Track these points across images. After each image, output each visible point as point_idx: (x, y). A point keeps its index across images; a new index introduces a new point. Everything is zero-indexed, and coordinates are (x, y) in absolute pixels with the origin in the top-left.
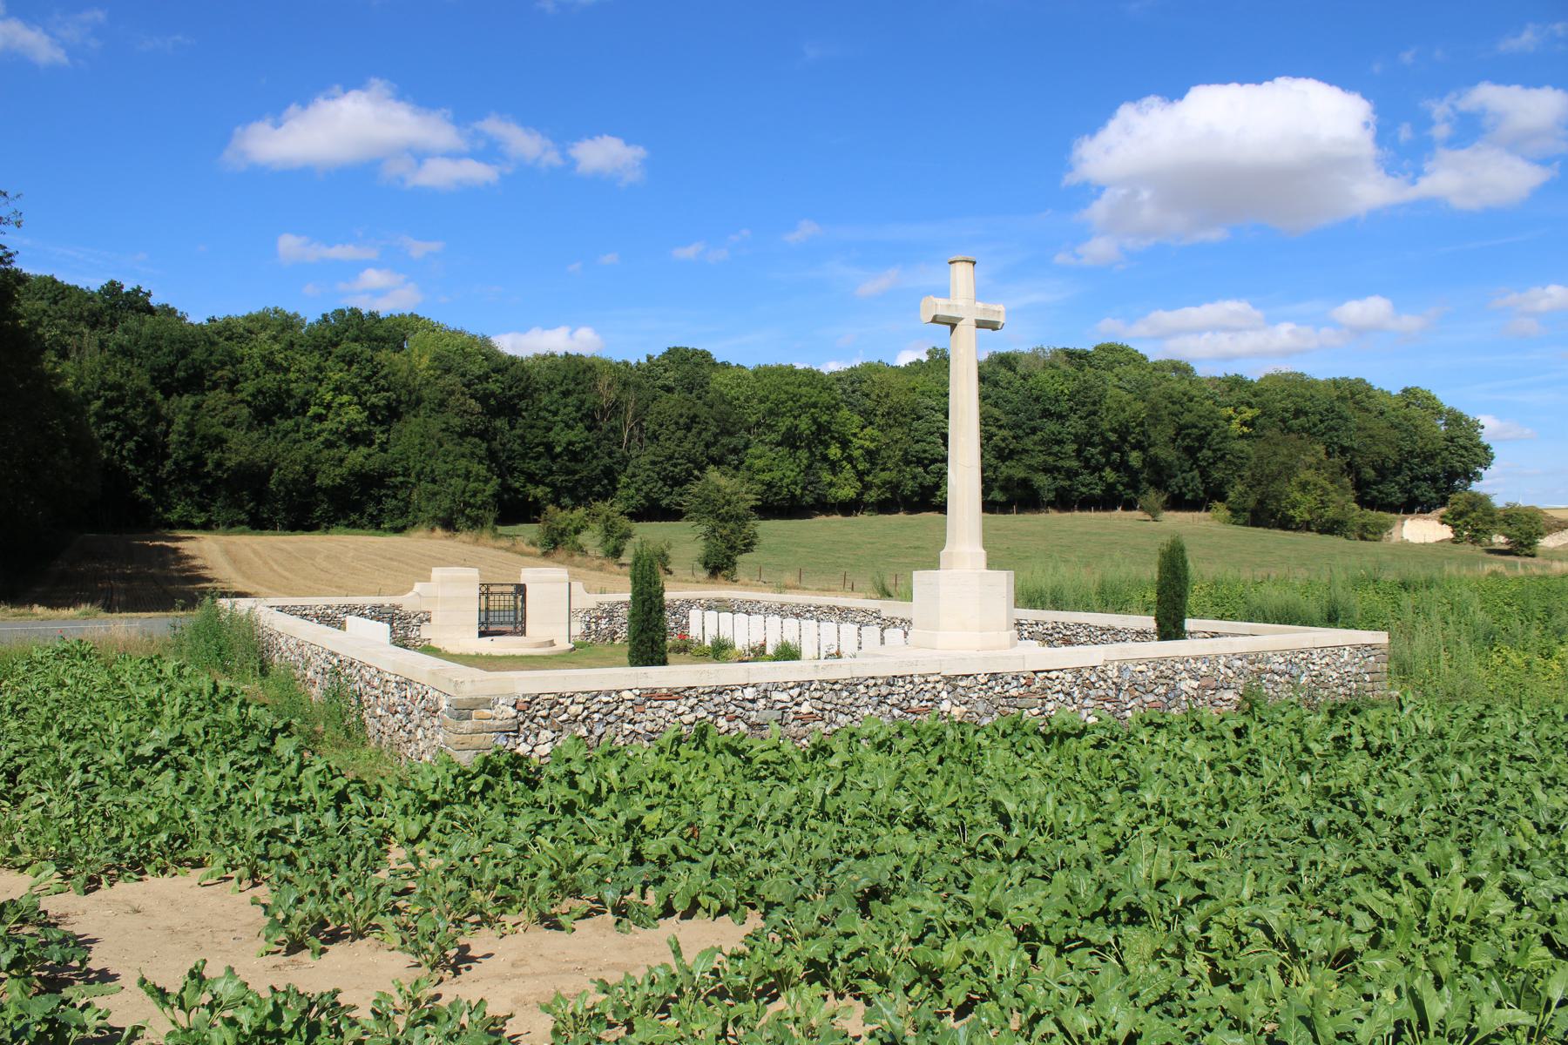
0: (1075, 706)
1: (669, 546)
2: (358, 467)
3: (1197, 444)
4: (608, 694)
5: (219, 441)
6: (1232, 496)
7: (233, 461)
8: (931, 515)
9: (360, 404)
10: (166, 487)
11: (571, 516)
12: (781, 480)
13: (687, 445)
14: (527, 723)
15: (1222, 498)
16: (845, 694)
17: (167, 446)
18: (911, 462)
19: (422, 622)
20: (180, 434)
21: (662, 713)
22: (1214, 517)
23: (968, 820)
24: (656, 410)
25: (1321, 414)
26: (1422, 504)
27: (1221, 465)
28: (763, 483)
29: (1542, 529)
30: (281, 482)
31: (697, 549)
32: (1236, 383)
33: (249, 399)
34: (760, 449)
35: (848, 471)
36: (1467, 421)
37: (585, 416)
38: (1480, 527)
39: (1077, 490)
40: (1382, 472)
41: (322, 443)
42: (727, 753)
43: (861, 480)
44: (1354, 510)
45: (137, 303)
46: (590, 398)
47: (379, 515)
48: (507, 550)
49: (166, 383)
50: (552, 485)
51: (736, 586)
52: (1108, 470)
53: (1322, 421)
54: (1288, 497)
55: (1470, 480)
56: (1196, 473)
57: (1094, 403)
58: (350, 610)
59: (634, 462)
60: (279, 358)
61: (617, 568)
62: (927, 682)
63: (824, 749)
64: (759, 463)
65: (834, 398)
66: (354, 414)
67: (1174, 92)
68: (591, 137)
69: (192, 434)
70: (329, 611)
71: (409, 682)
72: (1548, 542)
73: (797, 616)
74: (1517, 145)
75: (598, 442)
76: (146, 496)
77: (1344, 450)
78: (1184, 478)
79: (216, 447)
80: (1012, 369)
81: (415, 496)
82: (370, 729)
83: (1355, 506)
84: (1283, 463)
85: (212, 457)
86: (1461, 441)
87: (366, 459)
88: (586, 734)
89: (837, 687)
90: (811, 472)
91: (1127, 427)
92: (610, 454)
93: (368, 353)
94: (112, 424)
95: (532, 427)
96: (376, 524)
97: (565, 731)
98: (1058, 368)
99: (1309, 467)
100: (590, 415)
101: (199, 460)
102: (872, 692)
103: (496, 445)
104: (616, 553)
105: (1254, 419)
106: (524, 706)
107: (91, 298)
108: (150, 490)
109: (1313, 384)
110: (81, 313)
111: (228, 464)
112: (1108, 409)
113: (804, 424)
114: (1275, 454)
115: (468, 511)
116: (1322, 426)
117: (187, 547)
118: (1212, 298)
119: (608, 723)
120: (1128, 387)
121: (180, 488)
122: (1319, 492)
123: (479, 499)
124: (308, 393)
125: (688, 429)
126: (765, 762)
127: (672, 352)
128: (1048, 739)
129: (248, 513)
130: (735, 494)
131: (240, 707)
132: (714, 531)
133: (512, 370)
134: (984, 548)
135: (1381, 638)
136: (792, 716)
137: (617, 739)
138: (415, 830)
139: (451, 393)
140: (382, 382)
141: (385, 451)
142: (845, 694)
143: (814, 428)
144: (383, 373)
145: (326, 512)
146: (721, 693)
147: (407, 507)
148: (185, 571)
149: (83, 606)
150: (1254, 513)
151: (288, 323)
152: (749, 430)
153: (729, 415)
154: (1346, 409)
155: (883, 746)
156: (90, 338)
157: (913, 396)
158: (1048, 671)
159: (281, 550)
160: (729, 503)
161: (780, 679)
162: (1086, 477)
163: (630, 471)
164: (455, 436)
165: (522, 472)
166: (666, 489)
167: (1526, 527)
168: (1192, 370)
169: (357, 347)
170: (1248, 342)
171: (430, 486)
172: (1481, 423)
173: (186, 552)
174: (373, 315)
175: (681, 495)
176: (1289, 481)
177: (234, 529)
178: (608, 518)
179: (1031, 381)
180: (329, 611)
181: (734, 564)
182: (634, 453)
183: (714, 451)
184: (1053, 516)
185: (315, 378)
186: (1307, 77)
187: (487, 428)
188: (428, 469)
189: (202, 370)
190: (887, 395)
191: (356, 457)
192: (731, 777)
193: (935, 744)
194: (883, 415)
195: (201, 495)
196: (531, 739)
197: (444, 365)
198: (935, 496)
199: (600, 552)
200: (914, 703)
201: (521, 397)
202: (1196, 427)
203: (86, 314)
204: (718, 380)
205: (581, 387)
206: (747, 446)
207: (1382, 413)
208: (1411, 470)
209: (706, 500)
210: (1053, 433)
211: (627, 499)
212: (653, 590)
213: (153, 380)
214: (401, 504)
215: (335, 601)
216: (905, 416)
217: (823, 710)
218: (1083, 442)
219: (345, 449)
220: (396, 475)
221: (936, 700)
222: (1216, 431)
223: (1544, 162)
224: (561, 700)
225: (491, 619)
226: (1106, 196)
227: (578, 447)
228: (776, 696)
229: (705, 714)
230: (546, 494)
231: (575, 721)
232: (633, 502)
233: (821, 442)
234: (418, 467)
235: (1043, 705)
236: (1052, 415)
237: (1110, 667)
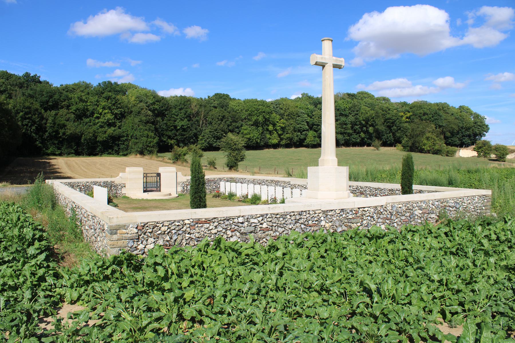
0: (374, 222)
1: (215, 160)
2: (111, 134)
3: (392, 125)
4: (179, 222)
5: (64, 126)
6: (403, 142)
7: (69, 132)
8: (303, 148)
10: (46, 141)
11: (183, 150)
12: (253, 137)
13: (221, 126)
14: (143, 235)
15: (400, 142)
16: (281, 219)
17: (46, 128)
18: (296, 131)
19: (122, 187)
20: (51, 123)
21: (203, 229)
22: (397, 149)
23: (348, 290)
24: (211, 114)
26: (465, 144)
27: (399, 131)
28: (247, 138)
29: (507, 152)
30: (85, 139)
31: (225, 160)
32: (405, 104)
33: (74, 112)
34: (246, 127)
35: (275, 134)
36: (480, 117)
37: (188, 116)
39: (351, 140)
40: (453, 134)
41: (99, 126)
42: (230, 251)
43: (280, 137)
44: (444, 146)
45: (36, 80)
46: (189, 111)
47: (119, 150)
48: (161, 161)
49: (46, 107)
50: (177, 139)
51: (238, 173)
53: (433, 117)
54: (422, 142)
55: (482, 136)
56: (391, 134)
57: (357, 111)
58: (95, 183)
59: (204, 131)
60: (84, 98)
62: (315, 213)
63: (274, 247)
64: (245, 132)
65: (270, 110)
66: (109, 116)
67: (381, 9)
68: (190, 26)
69: (54, 124)
70: (88, 184)
71: (95, 216)
72: (509, 157)
73: (260, 184)
74: (496, 26)
75: (192, 125)
76: (39, 145)
77: (440, 126)
78: (387, 136)
79: (63, 128)
82: (84, 234)
83: (445, 145)
84: (421, 131)
85: (61, 131)
86: (479, 124)
87: (114, 131)
88: (169, 239)
89: (278, 216)
90: (263, 134)
91: (368, 119)
93: (114, 96)
94: (27, 120)
95: (170, 120)
96: (117, 153)
97: (160, 238)
98: (345, 99)
99: (430, 132)
100: (189, 116)
101: (57, 132)
102: (293, 218)
103: (158, 126)
106: (141, 228)
107: (20, 78)
108: (41, 143)
109: (430, 104)
110: (16, 83)
111: (67, 134)
112: (362, 113)
113: (261, 119)
114: (418, 127)
115: (148, 148)
116: (433, 119)
117: (53, 162)
118: (395, 77)
119: (179, 234)
120: (368, 106)
121: (51, 142)
122: (433, 140)
123: (152, 144)
124: (94, 109)
125: (222, 120)
126: (247, 255)
127: (216, 95)
128: (370, 239)
129: (74, 150)
130: (237, 141)
131: (20, 229)
132: (230, 154)
133: (163, 101)
134: (337, 157)
135: (489, 192)
136: (259, 229)
137: (183, 241)
138: (75, 295)
139: (142, 109)
141: (120, 129)
142: (281, 219)
143: (264, 120)
144: (119, 102)
145: (101, 149)
146: (228, 220)
148: (51, 170)
149: (3, 183)
150: (411, 147)
151: (87, 86)
152: (242, 121)
153: (236, 115)
154: (441, 113)
155: (300, 245)
156: (19, 91)
157: (297, 109)
158: (364, 208)
159: (85, 162)
160: (235, 144)
161: (254, 213)
162: (355, 136)
163: (202, 134)
164: (144, 123)
165: (166, 135)
166: (215, 140)
167: (502, 152)
168: (390, 100)
169: (110, 94)
170: (406, 92)
171: (135, 140)
172: (485, 117)
173: (53, 163)
174: (116, 83)
175: (220, 142)
177: (70, 155)
178: (195, 150)
180: (88, 184)
181: (237, 165)
182: (204, 128)
183: (230, 128)
185: (96, 104)
186: (426, 4)
187: (154, 121)
188: (135, 135)
189: (58, 102)
190: (288, 109)
191: (111, 131)
192: (232, 264)
193: (322, 243)
194: (287, 115)
195: (58, 144)
196: (145, 242)
198: (304, 142)
200: (310, 222)
201: (166, 110)
202: (391, 119)
203: (18, 84)
204: (232, 104)
205: (186, 107)
206: (241, 126)
207: (452, 114)
208: (462, 133)
209: (228, 144)
210: (343, 121)
211: (202, 144)
212: (200, 175)
213: (41, 106)
214: (126, 146)
215: (90, 180)
216: (294, 116)
217: (272, 226)
218: (353, 124)
219: (106, 128)
220: (124, 137)
221: (319, 221)
223: (505, 32)
224: (158, 225)
225: (148, 186)
226: (359, 45)
227: (185, 127)
228: (252, 221)
229: (221, 229)
230: (175, 142)
231: (164, 234)
232: (204, 145)
233: (267, 125)
234: (131, 134)
235: (362, 222)
236: (343, 115)
237: (388, 206)
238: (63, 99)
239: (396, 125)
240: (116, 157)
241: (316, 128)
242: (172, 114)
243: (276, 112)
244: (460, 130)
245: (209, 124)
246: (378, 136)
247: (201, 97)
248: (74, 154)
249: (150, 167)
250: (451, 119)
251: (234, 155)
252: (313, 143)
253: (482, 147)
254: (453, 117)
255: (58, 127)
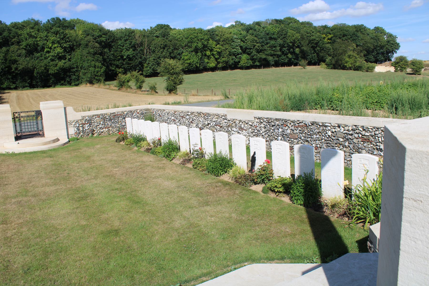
6: (327, 60)
7: (21, 67)
9: (61, 47)
11: (126, 77)
12: (193, 62)
13: (164, 53)
15: (324, 61)
24: (154, 43)
25: (351, 36)
26: (379, 61)
27: (323, 51)
30: (38, 73)
32: (325, 27)
33: (25, 47)
35: (212, 59)
36: (393, 36)
38: (404, 66)
41: (50, 60)
43: (217, 61)
46: (134, 41)
48: (108, 89)
50: (124, 68)
52: (289, 54)
53: (351, 38)
57: (285, 35)
59: (148, 59)
61: (140, 92)
64: (186, 58)
66: (59, 50)
69: (6, 60)
78: (312, 56)
80: (260, 26)
81: (81, 74)
85: (14, 66)
86: (392, 42)
92: (141, 58)
93: (62, 31)
95: (117, 51)
96: (70, 84)
101: (10, 68)
103: (106, 57)
104: (140, 87)
105: (332, 37)
109: (349, 26)
111: (19, 68)
114: (341, 47)
115: (96, 78)
121: (5, 77)
122: (354, 58)
123: (99, 73)
124: (44, 44)
125: (164, 48)
127: (158, 25)
129: (28, 83)
130: (175, 66)
132: (169, 78)
133: (109, 34)
139: (89, 42)
140: (67, 40)
141: (70, 61)
144: (67, 37)
145: (53, 81)
147: (79, 78)
150: (334, 65)
151: (37, 23)
152: (182, 48)
154: (359, 34)
160: (173, 69)
162: (283, 57)
163: (147, 62)
164: (92, 55)
165: (114, 65)
167: (419, 66)
169: (59, 29)
172: (397, 37)
174: (64, 19)
176: (345, 55)
178: (137, 77)
179: (265, 29)
181: (176, 89)
182: (148, 57)
184: (274, 69)
185: (46, 40)
189: (8, 39)
191: (61, 63)
194: (222, 41)
195: (12, 78)
197: (87, 33)
199: (135, 88)
201: (112, 42)
205: (130, 38)
206: (182, 53)
207: (368, 35)
208: (377, 51)
209: (166, 68)
214: (77, 77)
218: (282, 46)
219: (57, 61)
220: (74, 68)
222: (320, 42)
227: (131, 56)
230: (122, 71)
232: (149, 71)
234: (81, 65)
238: (13, 36)
239: (319, 46)
240: (69, 87)
241: (249, 51)
242: (118, 45)
243: (213, 38)
244: (375, 49)
245: (152, 52)
246: (303, 56)
247: (144, 28)
248: (29, 87)
249: (96, 95)
250: (368, 38)
251: (173, 79)
252: (247, 65)
253: (400, 62)
254: (369, 37)
255: (9, 63)
